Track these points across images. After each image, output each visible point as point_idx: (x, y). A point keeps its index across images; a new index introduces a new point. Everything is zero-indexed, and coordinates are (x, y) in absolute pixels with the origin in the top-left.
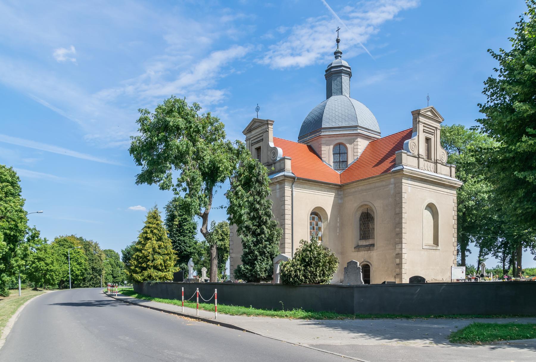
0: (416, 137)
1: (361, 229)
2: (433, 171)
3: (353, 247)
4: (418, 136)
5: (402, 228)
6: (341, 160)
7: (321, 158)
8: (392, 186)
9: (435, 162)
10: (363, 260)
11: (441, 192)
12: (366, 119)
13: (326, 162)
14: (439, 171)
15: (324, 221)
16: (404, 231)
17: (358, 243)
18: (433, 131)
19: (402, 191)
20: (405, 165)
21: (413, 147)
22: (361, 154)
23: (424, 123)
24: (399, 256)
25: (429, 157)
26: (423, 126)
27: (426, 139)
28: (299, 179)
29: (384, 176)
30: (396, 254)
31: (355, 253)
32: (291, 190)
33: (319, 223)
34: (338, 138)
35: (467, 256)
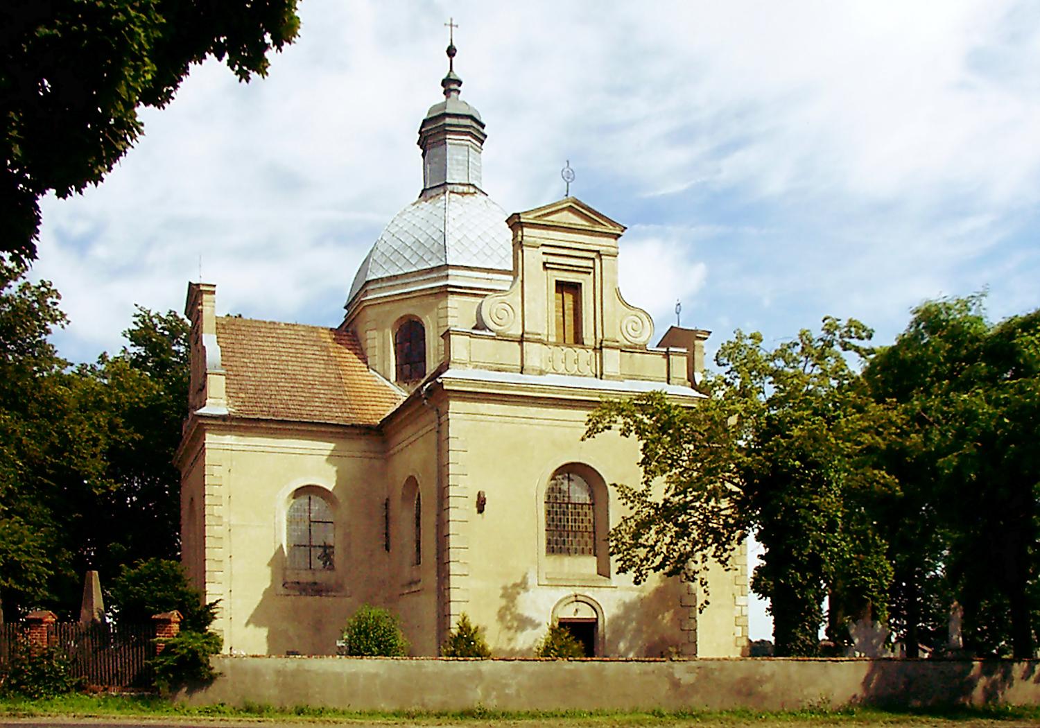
4: (522, 281)
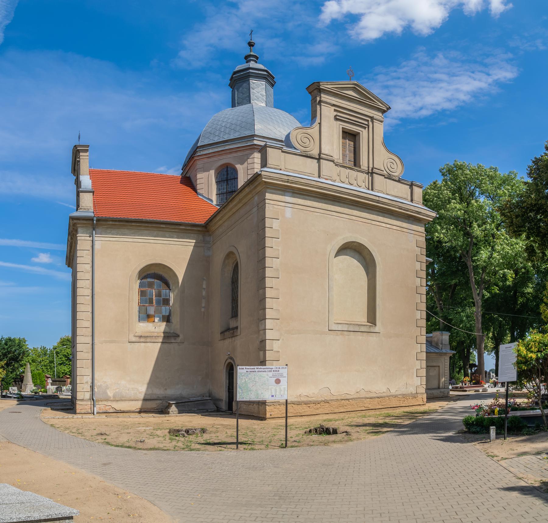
4: (320, 124)
7: (195, 190)
11: (384, 225)
13: (203, 196)
14: (376, 186)
15: (174, 287)
18: (366, 123)
21: (305, 140)
26: (334, 109)
30: (260, 342)
34: (221, 157)
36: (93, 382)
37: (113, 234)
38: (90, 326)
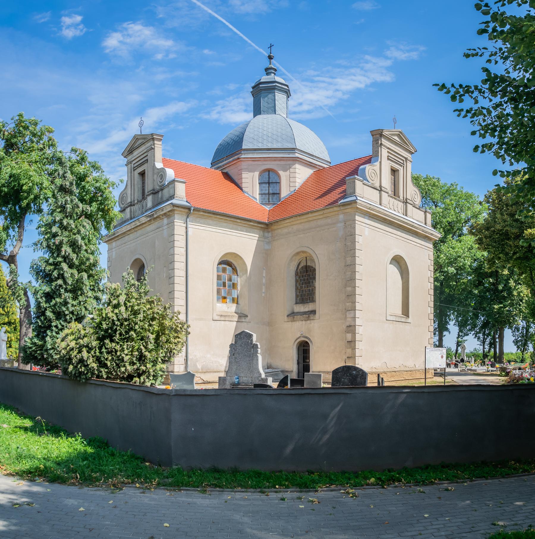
0: (377, 164)
1: (297, 288)
2: (401, 212)
3: (286, 315)
5: (355, 287)
6: (271, 192)
8: (341, 225)
9: (404, 202)
10: (299, 335)
11: (413, 243)
12: (308, 143)
13: (248, 194)
15: (241, 274)
16: (358, 291)
17: (293, 309)
18: (402, 162)
19: (355, 232)
20: (360, 197)
21: (373, 175)
22: (301, 185)
23: (388, 148)
24: (351, 329)
25: (395, 194)
27: (391, 169)
28: (196, 210)
29: (329, 210)
30: (347, 326)
31: (288, 323)
32: (185, 225)
33: (234, 277)
34: (266, 163)
35: (444, 336)
36: (187, 356)
37: (201, 223)
38: (184, 304)
